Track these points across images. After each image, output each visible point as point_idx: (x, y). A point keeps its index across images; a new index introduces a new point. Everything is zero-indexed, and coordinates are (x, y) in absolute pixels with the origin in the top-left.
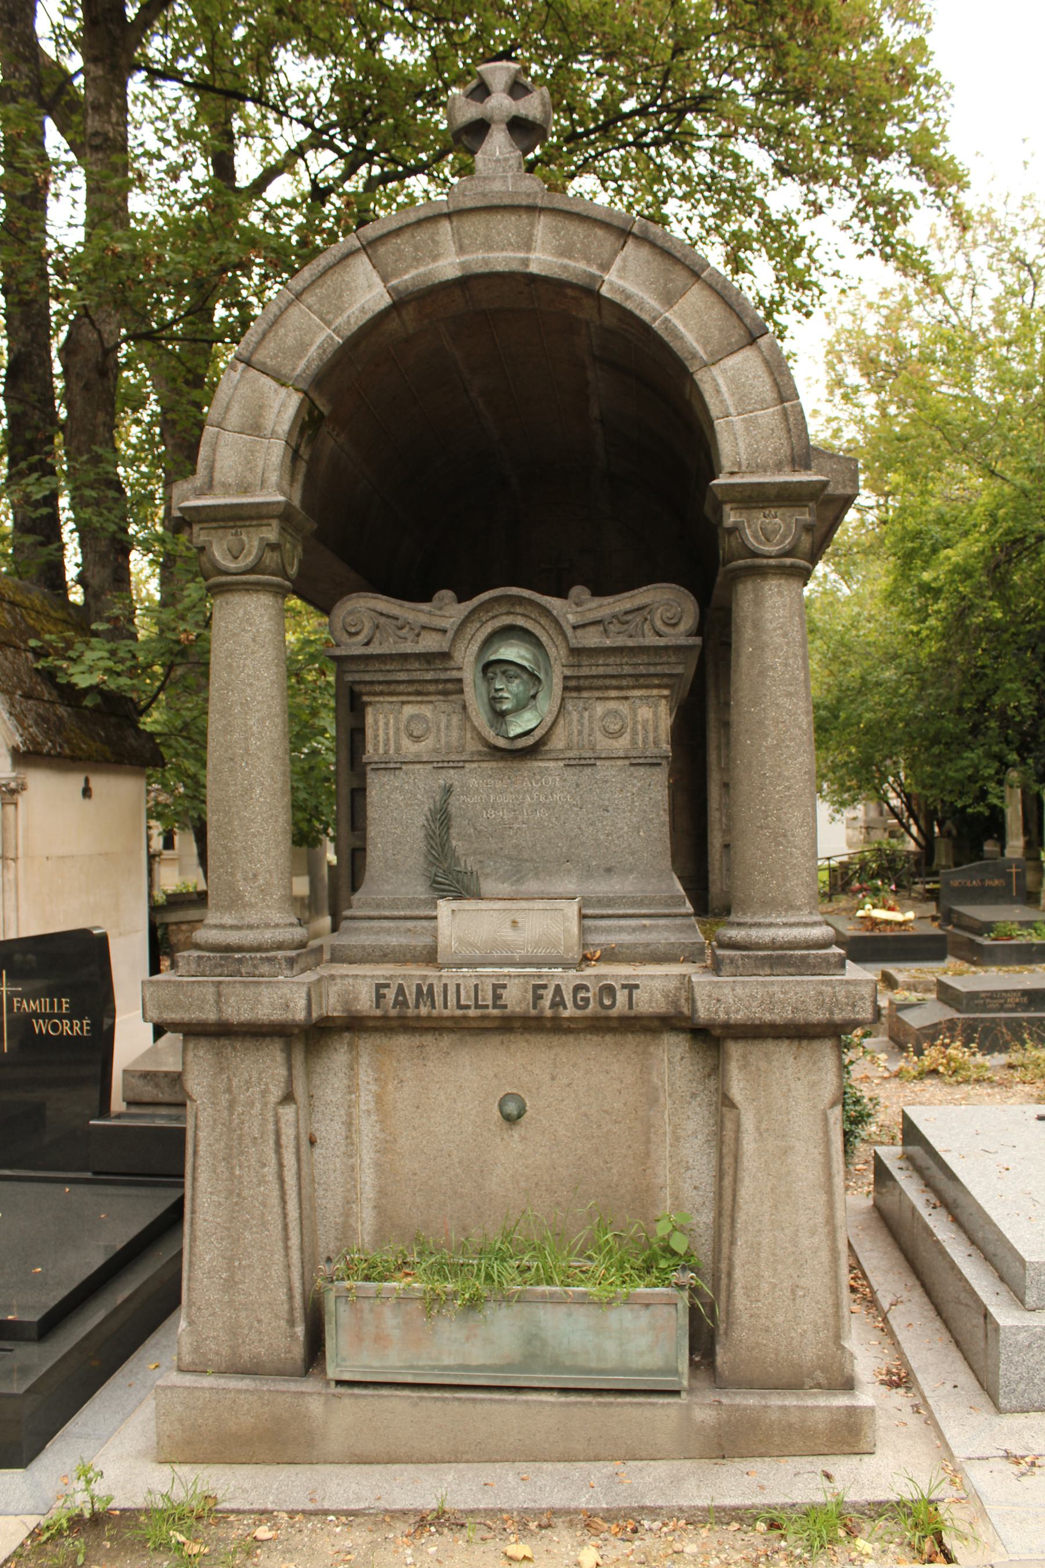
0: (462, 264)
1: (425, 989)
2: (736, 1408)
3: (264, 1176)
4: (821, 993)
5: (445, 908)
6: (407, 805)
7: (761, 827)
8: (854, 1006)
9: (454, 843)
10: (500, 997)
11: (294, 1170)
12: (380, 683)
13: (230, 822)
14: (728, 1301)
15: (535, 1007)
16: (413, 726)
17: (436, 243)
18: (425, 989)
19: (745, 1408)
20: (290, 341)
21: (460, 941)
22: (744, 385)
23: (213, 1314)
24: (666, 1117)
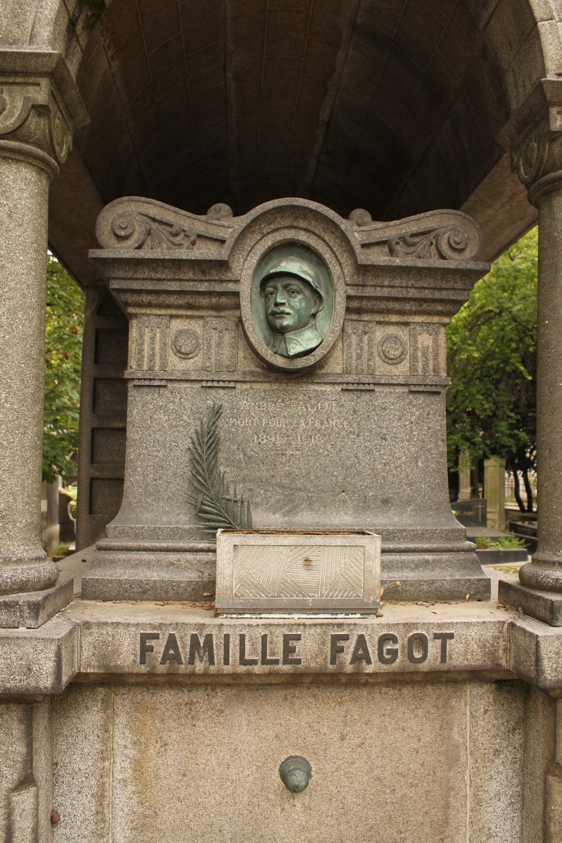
1: (202, 641)
5: (225, 542)
6: (171, 427)
9: (222, 468)
10: (293, 650)
12: (149, 292)
15: (333, 662)
16: (181, 341)
18: (202, 641)
21: (243, 582)
24: (467, 778)
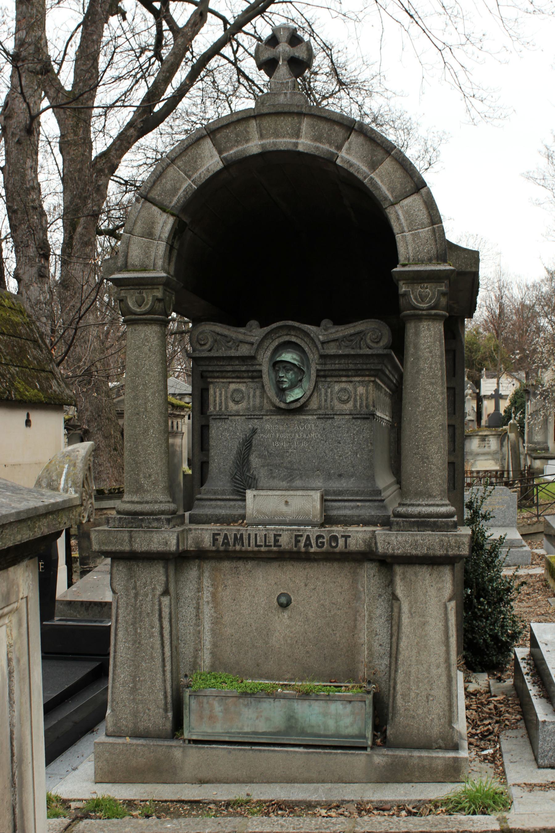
0: (262, 146)
1: (239, 536)
2: (396, 757)
3: (153, 633)
4: (442, 541)
6: (231, 439)
7: (415, 454)
8: (459, 547)
10: (278, 541)
11: (168, 630)
12: (217, 372)
13: (137, 447)
14: (393, 702)
15: (296, 546)
16: (235, 395)
17: (248, 132)
18: (239, 536)
19: (400, 757)
20: (168, 186)
21: (258, 511)
22: (412, 215)
23: (125, 706)
